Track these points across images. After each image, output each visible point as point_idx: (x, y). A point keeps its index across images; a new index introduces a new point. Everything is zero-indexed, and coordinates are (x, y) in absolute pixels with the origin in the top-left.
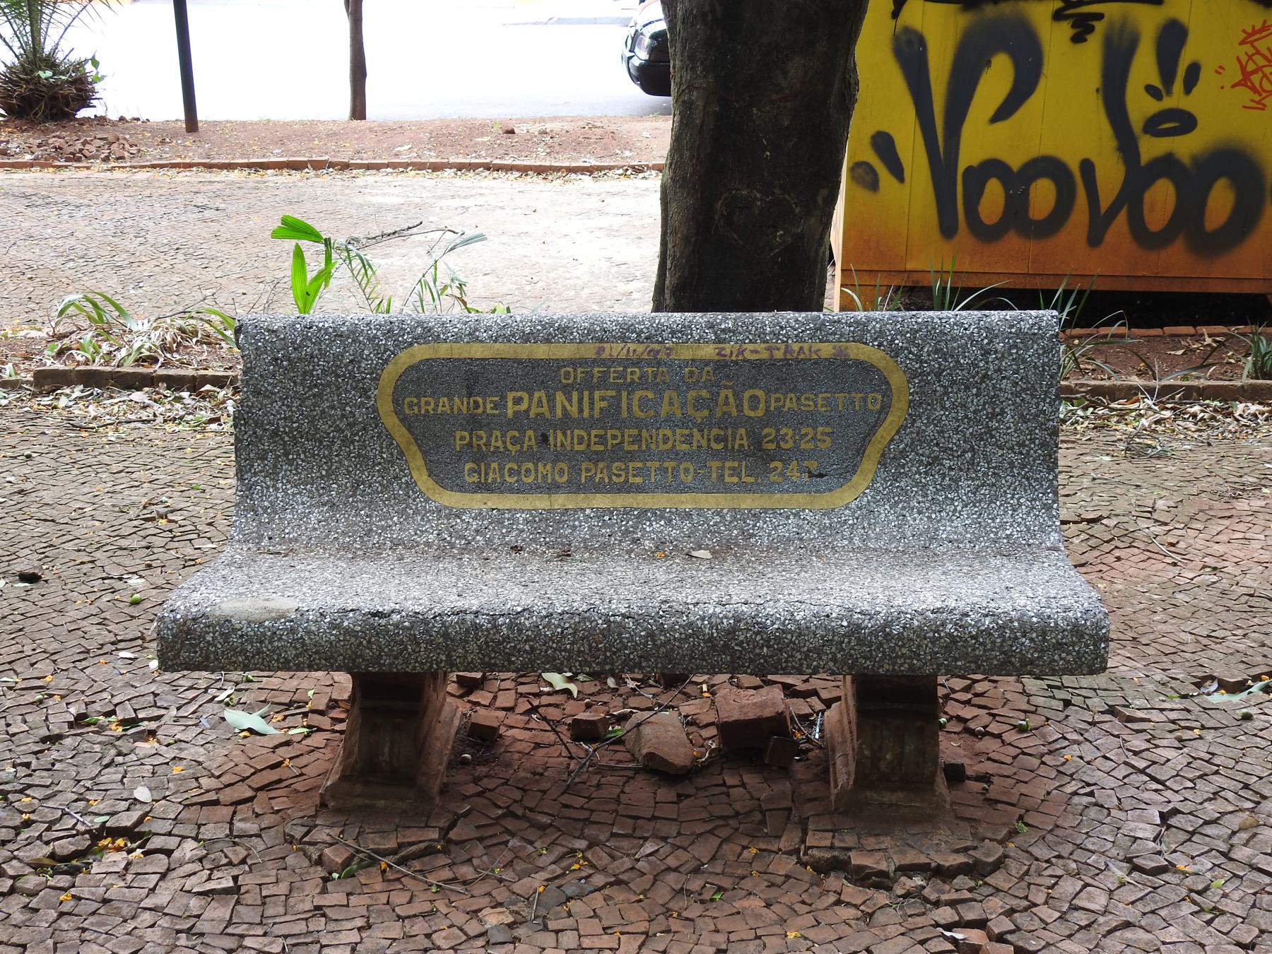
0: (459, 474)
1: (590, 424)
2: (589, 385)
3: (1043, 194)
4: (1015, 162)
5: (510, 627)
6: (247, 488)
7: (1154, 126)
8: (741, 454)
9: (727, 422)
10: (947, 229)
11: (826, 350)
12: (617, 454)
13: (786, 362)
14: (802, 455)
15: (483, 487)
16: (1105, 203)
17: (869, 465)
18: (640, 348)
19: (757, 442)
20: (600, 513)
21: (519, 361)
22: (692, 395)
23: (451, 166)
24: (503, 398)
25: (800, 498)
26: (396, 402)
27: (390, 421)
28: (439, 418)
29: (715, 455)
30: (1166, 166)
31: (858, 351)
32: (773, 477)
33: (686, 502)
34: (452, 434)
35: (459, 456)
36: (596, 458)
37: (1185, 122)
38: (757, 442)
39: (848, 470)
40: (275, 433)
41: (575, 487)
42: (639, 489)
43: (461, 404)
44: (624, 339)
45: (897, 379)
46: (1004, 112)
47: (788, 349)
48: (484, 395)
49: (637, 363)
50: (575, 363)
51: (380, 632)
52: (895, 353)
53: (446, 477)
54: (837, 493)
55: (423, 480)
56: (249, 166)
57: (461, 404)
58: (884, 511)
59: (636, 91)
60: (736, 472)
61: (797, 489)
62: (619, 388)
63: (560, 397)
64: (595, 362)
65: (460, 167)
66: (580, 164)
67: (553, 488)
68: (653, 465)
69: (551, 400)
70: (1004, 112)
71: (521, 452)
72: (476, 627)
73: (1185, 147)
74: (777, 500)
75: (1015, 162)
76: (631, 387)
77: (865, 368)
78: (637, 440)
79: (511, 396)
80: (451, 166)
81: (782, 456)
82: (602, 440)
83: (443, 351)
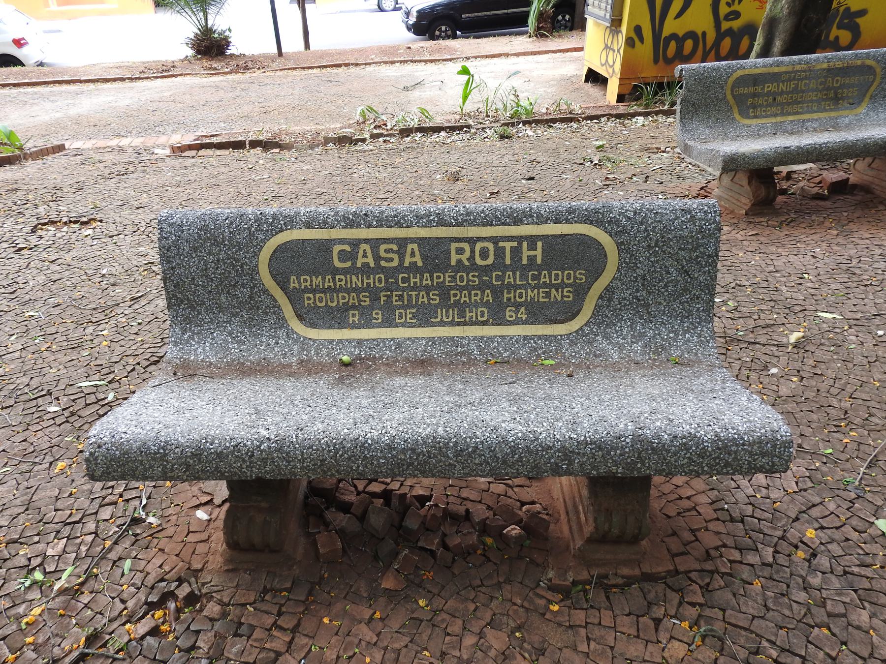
0: (748, 114)
1: (788, 93)
2: (790, 80)
3: (689, 44)
4: (681, 34)
5: (825, 147)
6: (684, 125)
7: (727, 18)
8: (832, 99)
9: (828, 89)
10: (656, 61)
11: (859, 62)
12: (797, 102)
13: (847, 67)
14: (848, 97)
15: (756, 117)
16: (708, 47)
17: (867, 99)
18: (805, 66)
19: (836, 94)
20: (792, 121)
21: (769, 74)
22: (820, 80)
23: (398, 62)
24: (764, 87)
25: (847, 112)
26: (732, 91)
27: (729, 97)
28: (744, 95)
29: (823, 100)
30: (730, 31)
31: (869, 62)
32: (840, 106)
33: (815, 116)
34: (747, 100)
35: (748, 107)
36: (789, 104)
37: (737, 15)
38: (836, 94)
39: (860, 103)
40: (694, 104)
41: (783, 114)
42: (801, 113)
43: (751, 90)
44: (800, 64)
45: (878, 70)
46: (679, 15)
47: (848, 63)
48: (758, 86)
49: (804, 71)
50: (786, 73)
51: (789, 153)
52: (878, 62)
53: (744, 114)
54: (858, 109)
55: (737, 116)
56: (319, 67)
57: (751, 90)
58: (871, 113)
59: (411, 35)
60: (829, 105)
61: (846, 109)
62: (798, 80)
63: (781, 84)
64: (792, 72)
65: (401, 62)
66: (444, 58)
67: (775, 115)
68: (805, 105)
69: (778, 86)
70: (679, 15)
71: (767, 105)
72: (816, 148)
73: (736, 24)
74: (841, 113)
75: (681, 34)
76: (802, 80)
77: (870, 68)
78: (802, 97)
79: (766, 85)
80: (398, 62)
81: (843, 99)
82: (792, 98)
83: (747, 72)
